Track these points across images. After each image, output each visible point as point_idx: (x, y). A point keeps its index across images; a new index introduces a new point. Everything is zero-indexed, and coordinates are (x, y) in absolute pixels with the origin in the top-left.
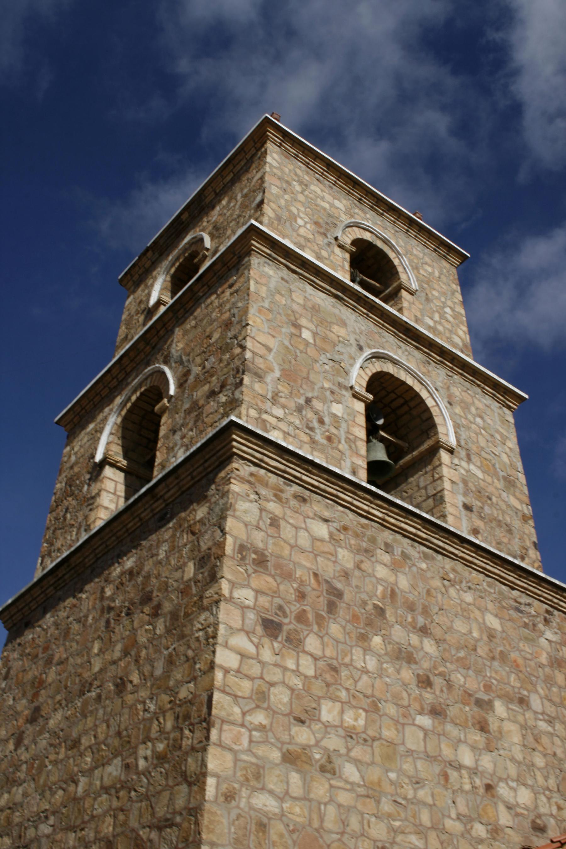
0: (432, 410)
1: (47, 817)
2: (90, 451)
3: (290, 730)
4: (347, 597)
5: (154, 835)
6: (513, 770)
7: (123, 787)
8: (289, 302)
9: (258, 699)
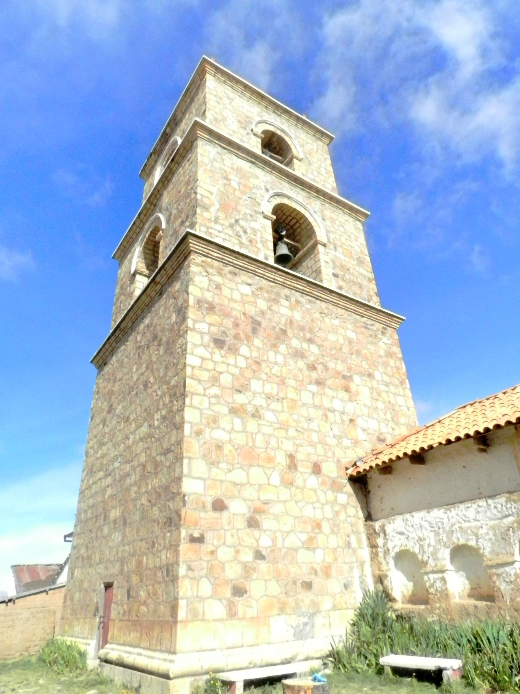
1: (117, 459)
3: (233, 396)
5: (163, 458)
6: (365, 411)
7: (148, 437)
8: (222, 166)
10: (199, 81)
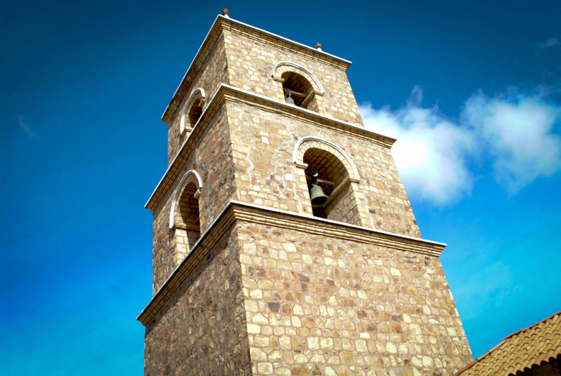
0: (343, 162)
2: (166, 222)
3: (293, 358)
4: (311, 280)
9: (274, 346)
10: (217, 36)
